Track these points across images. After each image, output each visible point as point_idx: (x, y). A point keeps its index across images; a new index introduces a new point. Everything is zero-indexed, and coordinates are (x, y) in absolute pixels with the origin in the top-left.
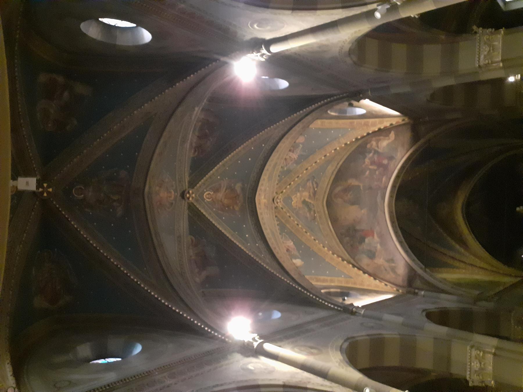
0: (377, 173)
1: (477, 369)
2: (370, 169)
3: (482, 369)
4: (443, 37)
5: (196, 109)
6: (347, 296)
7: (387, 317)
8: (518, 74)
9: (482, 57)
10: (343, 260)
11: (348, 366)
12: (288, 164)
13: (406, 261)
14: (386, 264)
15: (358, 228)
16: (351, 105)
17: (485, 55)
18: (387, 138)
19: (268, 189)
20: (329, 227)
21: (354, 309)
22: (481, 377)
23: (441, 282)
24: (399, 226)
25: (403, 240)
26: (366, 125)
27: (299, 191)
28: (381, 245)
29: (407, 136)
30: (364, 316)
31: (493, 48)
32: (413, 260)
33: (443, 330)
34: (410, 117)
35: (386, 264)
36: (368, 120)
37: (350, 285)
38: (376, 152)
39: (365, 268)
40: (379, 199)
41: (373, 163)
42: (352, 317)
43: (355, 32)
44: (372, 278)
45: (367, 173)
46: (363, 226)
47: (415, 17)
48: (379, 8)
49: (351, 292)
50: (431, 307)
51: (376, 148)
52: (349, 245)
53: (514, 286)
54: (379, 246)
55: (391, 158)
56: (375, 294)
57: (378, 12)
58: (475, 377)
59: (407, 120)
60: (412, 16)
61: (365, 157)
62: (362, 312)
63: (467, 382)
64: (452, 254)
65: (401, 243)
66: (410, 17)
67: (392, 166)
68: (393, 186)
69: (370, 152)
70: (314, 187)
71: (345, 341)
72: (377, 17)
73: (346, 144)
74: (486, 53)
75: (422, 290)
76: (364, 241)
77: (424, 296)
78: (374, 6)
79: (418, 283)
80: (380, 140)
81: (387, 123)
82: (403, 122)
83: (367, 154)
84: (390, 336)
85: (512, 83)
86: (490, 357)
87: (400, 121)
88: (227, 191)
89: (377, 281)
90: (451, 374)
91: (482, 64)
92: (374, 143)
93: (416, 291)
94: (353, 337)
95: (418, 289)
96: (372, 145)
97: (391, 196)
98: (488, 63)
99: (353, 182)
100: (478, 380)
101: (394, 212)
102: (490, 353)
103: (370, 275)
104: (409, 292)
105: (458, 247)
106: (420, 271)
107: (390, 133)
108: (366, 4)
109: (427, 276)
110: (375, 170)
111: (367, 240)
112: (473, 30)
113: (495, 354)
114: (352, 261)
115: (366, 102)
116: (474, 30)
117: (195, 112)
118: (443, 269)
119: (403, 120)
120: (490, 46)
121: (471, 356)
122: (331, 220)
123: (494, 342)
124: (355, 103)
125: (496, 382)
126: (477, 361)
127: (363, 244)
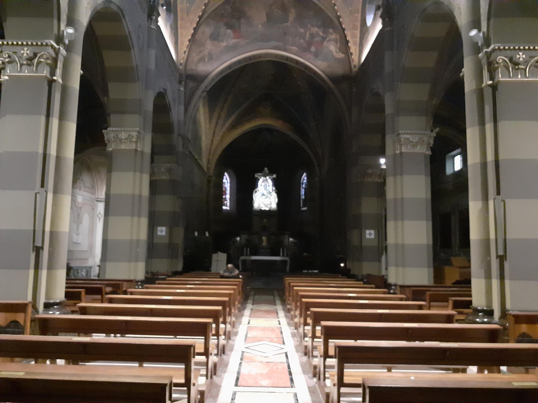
0: (302, 41)
1: (119, 136)
2: (306, 33)
3: (121, 140)
4: (434, 102)
6: (167, 9)
7: (153, 53)
8: (387, 166)
9: (408, 136)
10: (206, 5)
11: (92, 10)
13: (212, 72)
14: (206, 52)
15: (242, 21)
16: (378, 8)
17: (409, 139)
18: (338, 50)
21: (154, 17)
22: (113, 140)
23: (195, 106)
24: (247, 65)
25: (232, 69)
26: (354, 28)
28: (226, 47)
29: (339, 70)
30: (149, 28)
31: (414, 145)
32: (213, 80)
33: (150, 107)
34: (357, 73)
35: (206, 52)
36: (359, 29)
37: (179, 14)
38: (324, 39)
39: (200, 30)
40: (274, 43)
41: (312, 35)
42: (146, 16)
43: (459, 9)
44: (190, 37)
45: (302, 30)
47: (461, 72)
48: (481, 34)
49: (172, 15)
50: (170, 97)
51: (327, 39)
53: (200, 167)
54: (224, 44)
55: (316, 55)
56: (174, 41)
57: (477, 32)
58: (112, 135)
59: (355, 70)
60: (463, 70)
62: (153, 27)
63: (106, 129)
64: (223, 115)
65: (230, 67)
66: (463, 67)
67: (309, 56)
68: (287, 58)
71: (119, 7)
72: (471, 32)
73: (335, 5)
74: (411, 139)
75: (185, 88)
76: (228, 28)
77: (179, 90)
78: (484, 28)
79: (191, 84)
80: (337, 43)
81: (353, 49)
82: (353, 66)
84: (133, 56)
86: (133, 146)
87: (354, 63)
89: (188, 43)
90: (109, 115)
91: (402, 136)
92: (333, 36)
93: (183, 83)
94: (124, 16)
96: (332, 34)
97: (277, 56)
98: (401, 141)
99: (292, 15)
100: (110, 137)
101: (260, 60)
102: (137, 146)
103: (193, 35)
104: (181, 75)
105: (230, 121)
106: (203, 86)
107: (342, 53)
108: (489, 19)
109: (199, 92)
111: (229, 31)
112: (435, 128)
113: (136, 150)
114: (206, 15)
115: (379, 26)
116: (434, 130)
118: (208, 108)
119: (355, 66)
120: (417, 142)
121: (130, 131)
123: (148, 150)
124: (380, 13)
125: (112, 151)
126: (127, 136)
127: (226, 27)
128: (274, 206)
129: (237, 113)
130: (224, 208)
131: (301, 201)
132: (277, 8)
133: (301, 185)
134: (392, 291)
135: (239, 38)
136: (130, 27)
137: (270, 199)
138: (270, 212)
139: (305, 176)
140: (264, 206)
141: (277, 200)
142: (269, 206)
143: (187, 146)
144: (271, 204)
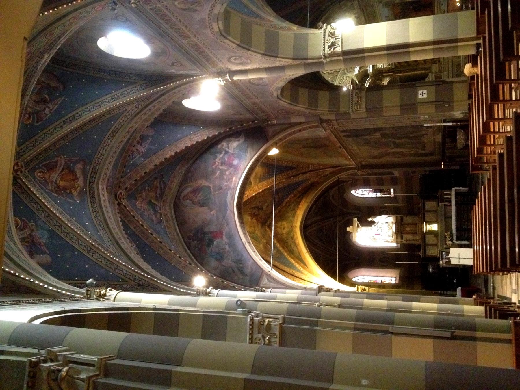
0: (227, 173)
5: (46, 56)
12: (135, 157)
14: (234, 265)
15: (206, 230)
19: (111, 179)
20: (176, 230)
27: (145, 190)
46: (213, 228)
52: (197, 249)
69: (221, 153)
70: (161, 188)
83: (218, 155)
85: (436, 222)
88: (64, 172)
95: (265, 287)
99: (203, 183)
110: (226, 171)
111: (215, 243)
117: (43, 61)
128: (391, 219)
129: (288, 257)
131: (383, 196)
132: (196, 197)
133: (364, 196)
135: (222, 234)
136: (283, 102)
138: (397, 223)
141: (384, 216)
142: (391, 225)
144: (387, 223)
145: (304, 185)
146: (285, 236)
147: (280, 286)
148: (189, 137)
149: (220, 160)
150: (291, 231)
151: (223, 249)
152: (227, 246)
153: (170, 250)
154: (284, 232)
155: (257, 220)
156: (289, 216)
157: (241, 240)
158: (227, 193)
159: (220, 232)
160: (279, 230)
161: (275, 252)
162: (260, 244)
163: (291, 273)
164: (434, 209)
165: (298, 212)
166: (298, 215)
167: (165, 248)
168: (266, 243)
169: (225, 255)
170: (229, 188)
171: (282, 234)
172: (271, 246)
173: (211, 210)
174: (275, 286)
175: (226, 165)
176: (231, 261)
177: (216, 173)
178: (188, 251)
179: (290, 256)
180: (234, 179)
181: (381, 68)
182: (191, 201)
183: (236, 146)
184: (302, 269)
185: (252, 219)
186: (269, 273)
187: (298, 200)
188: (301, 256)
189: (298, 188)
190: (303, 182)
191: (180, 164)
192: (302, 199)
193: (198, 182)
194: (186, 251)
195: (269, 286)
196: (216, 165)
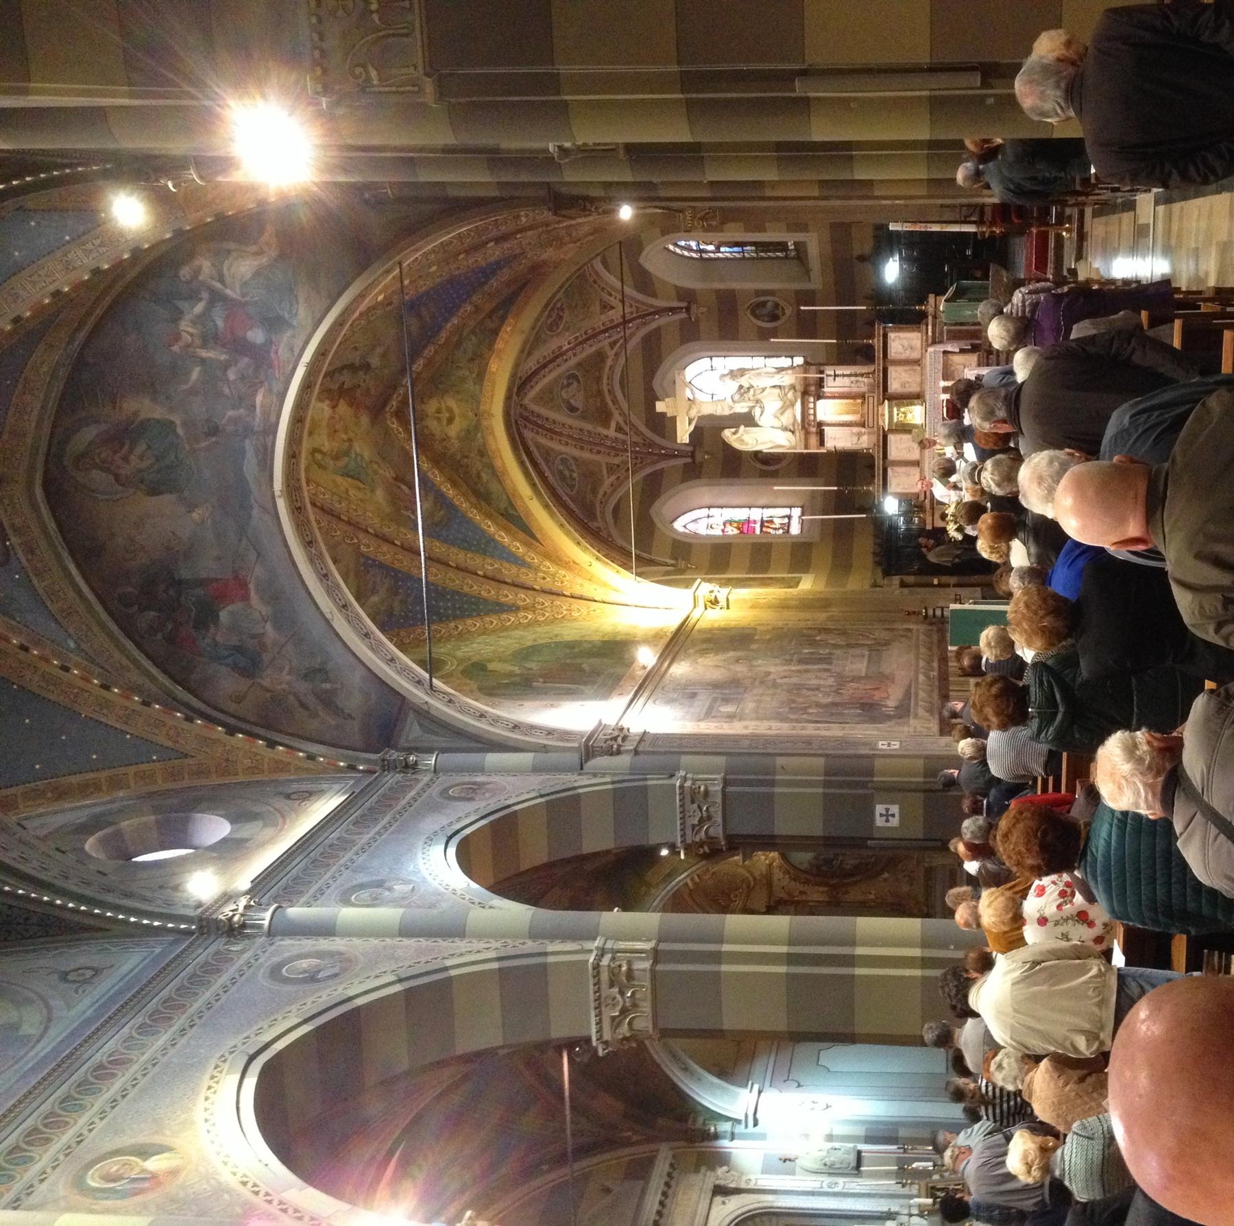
0: (232, 375)
2: (203, 361)
14: (302, 687)
15: (184, 573)
28: (278, 627)
35: (302, 687)
38: (216, 298)
45: (196, 373)
46: (207, 566)
61: (177, 316)
64: (490, 565)
69: (193, 297)
75: (430, 751)
96: (197, 272)
99: (146, 408)
105: (504, 538)
110: (226, 366)
111: (224, 616)
122: (72, 553)
130: (795, 529)
134: (1030, 783)
135: (243, 585)
137: (764, 390)
139: (676, 245)
140: (788, 413)
142: (790, 395)
143: (615, 739)
145: (505, 274)
146: (457, 444)
147: (465, 744)
148: (59, 254)
149: (193, 323)
150: (475, 430)
151: (254, 637)
152: (269, 627)
153: (65, 669)
154: (453, 431)
155: (351, 405)
156: (463, 379)
157: (318, 608)
158: (243, 452)
159: (236, 578)
160: (433, 425)
161: (426, 505)
162: (373, 491)
163: (489, 574)
164: (916, 355)
165: (493, 366)
166: (494, 373)
167: (43, 666)
168: (396, 479)
169: (266, 657)
170: (248, 431)
171: (446, 438)
172: (412, 488)
173: (191, 507)
174: (450, 745)
175: (223, 346)
176: (289, 673)
177: (189, 373)
178: (130, 645)
179: (480, 510)
180: (259, 399)
181: (771, 851)
182: (108, 470)
183: (249, 275)
184: (519, 549)
185: (334, 407)
186: (425, 707)
187: (490, 325)
188: (516, 510)
189: (485, 283)
190: (497, 266)
191: (41, 347)
192: (503, 319)
193: (125, 405)
194: (123, 650)
195: (425, 744)
196: (181, 343)
